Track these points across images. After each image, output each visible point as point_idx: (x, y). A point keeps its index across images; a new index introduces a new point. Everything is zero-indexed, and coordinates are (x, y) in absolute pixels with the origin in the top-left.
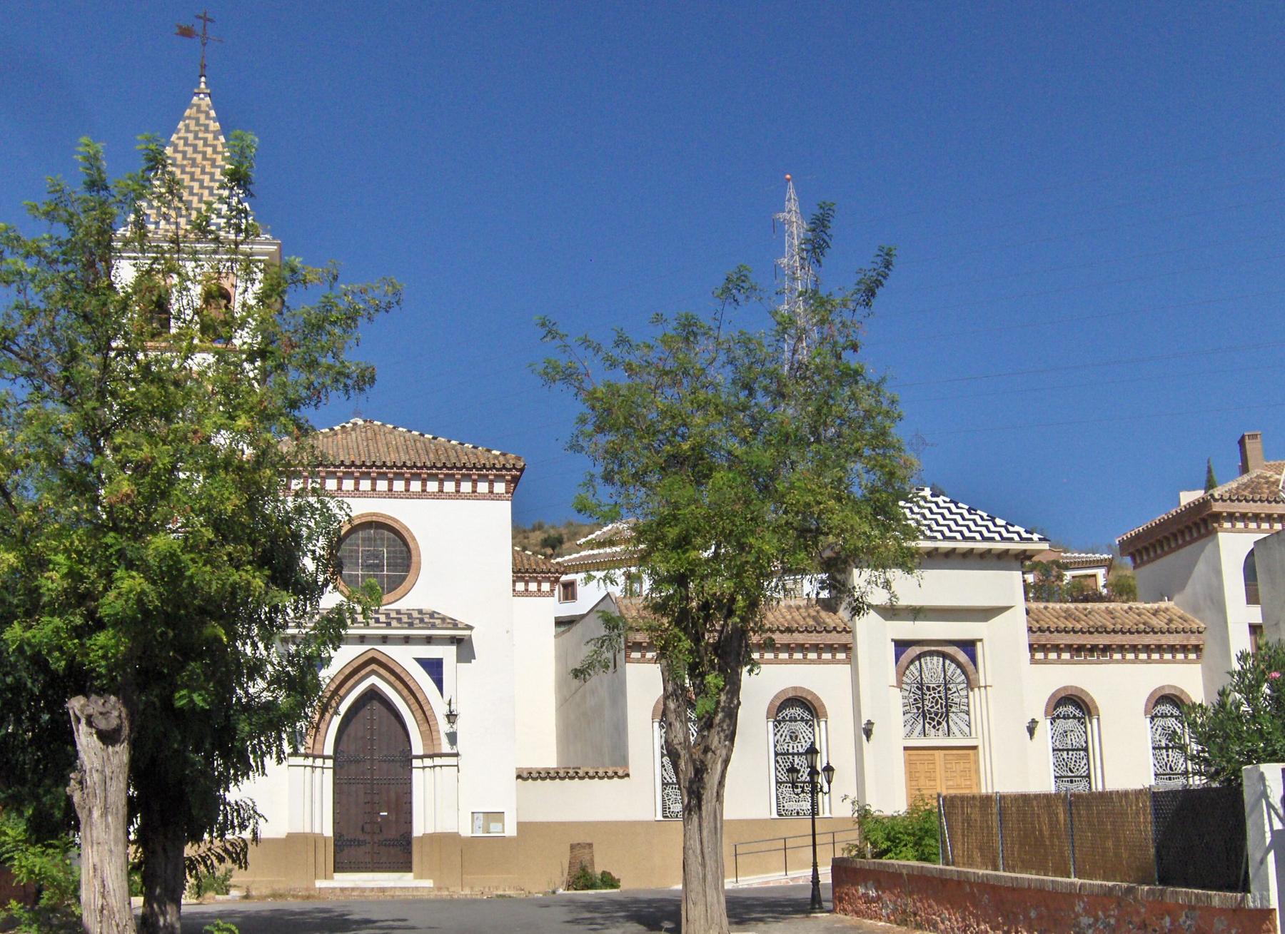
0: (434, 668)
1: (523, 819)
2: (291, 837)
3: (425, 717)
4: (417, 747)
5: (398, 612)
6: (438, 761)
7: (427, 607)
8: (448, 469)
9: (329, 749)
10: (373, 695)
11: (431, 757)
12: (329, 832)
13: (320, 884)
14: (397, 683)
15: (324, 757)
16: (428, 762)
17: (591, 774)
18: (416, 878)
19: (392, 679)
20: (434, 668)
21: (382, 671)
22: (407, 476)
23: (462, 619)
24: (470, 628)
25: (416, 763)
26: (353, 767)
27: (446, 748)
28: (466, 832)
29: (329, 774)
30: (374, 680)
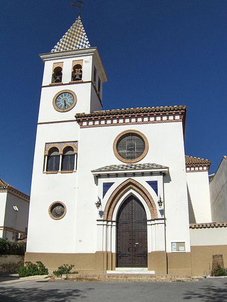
0: (154, 185)
1: (192, 245)
2: (97, 252)
3: (151, 205)
4: (149, 217)
5: (140, 165)
6: (156, 222)
7: (151, 162)
8: (157, 112)
9: (114, 219)
10: (132, 197)
11: (154, 220)
12: (114, 251)
13: (109, 272)
14: (140, 192)
15: (112, 222)
16: (153, 222)
17: (221, 225)
18: (149, 270)
19: (138, 190)
20: (154, 185)
21: (134, 187)
22: (124, 117)
23: (164, 165)
24: (168, 168)
25: (148, 223)
26: (125, 225)
27: (159, 216)
28: (169, 250)
29: (114, 228)
30: (131, 191)
